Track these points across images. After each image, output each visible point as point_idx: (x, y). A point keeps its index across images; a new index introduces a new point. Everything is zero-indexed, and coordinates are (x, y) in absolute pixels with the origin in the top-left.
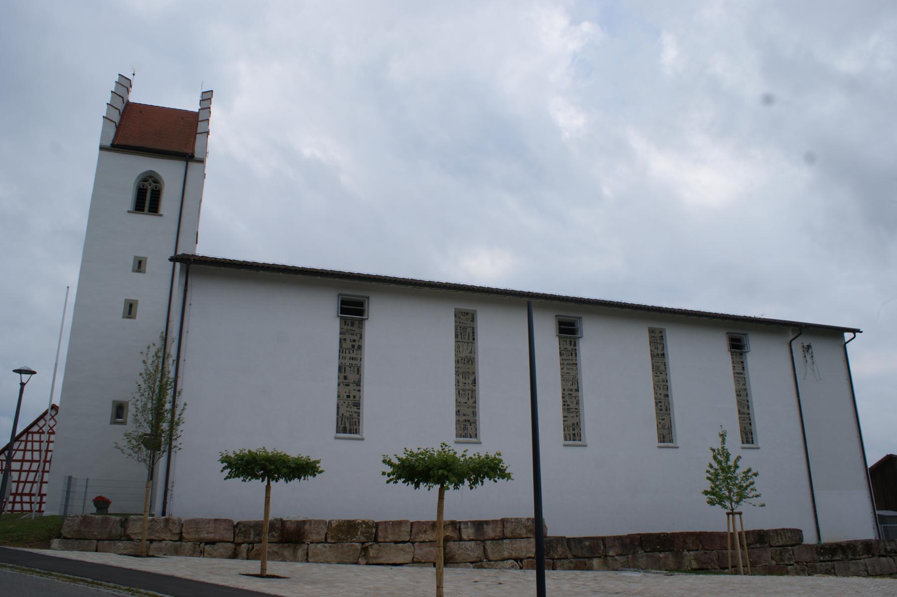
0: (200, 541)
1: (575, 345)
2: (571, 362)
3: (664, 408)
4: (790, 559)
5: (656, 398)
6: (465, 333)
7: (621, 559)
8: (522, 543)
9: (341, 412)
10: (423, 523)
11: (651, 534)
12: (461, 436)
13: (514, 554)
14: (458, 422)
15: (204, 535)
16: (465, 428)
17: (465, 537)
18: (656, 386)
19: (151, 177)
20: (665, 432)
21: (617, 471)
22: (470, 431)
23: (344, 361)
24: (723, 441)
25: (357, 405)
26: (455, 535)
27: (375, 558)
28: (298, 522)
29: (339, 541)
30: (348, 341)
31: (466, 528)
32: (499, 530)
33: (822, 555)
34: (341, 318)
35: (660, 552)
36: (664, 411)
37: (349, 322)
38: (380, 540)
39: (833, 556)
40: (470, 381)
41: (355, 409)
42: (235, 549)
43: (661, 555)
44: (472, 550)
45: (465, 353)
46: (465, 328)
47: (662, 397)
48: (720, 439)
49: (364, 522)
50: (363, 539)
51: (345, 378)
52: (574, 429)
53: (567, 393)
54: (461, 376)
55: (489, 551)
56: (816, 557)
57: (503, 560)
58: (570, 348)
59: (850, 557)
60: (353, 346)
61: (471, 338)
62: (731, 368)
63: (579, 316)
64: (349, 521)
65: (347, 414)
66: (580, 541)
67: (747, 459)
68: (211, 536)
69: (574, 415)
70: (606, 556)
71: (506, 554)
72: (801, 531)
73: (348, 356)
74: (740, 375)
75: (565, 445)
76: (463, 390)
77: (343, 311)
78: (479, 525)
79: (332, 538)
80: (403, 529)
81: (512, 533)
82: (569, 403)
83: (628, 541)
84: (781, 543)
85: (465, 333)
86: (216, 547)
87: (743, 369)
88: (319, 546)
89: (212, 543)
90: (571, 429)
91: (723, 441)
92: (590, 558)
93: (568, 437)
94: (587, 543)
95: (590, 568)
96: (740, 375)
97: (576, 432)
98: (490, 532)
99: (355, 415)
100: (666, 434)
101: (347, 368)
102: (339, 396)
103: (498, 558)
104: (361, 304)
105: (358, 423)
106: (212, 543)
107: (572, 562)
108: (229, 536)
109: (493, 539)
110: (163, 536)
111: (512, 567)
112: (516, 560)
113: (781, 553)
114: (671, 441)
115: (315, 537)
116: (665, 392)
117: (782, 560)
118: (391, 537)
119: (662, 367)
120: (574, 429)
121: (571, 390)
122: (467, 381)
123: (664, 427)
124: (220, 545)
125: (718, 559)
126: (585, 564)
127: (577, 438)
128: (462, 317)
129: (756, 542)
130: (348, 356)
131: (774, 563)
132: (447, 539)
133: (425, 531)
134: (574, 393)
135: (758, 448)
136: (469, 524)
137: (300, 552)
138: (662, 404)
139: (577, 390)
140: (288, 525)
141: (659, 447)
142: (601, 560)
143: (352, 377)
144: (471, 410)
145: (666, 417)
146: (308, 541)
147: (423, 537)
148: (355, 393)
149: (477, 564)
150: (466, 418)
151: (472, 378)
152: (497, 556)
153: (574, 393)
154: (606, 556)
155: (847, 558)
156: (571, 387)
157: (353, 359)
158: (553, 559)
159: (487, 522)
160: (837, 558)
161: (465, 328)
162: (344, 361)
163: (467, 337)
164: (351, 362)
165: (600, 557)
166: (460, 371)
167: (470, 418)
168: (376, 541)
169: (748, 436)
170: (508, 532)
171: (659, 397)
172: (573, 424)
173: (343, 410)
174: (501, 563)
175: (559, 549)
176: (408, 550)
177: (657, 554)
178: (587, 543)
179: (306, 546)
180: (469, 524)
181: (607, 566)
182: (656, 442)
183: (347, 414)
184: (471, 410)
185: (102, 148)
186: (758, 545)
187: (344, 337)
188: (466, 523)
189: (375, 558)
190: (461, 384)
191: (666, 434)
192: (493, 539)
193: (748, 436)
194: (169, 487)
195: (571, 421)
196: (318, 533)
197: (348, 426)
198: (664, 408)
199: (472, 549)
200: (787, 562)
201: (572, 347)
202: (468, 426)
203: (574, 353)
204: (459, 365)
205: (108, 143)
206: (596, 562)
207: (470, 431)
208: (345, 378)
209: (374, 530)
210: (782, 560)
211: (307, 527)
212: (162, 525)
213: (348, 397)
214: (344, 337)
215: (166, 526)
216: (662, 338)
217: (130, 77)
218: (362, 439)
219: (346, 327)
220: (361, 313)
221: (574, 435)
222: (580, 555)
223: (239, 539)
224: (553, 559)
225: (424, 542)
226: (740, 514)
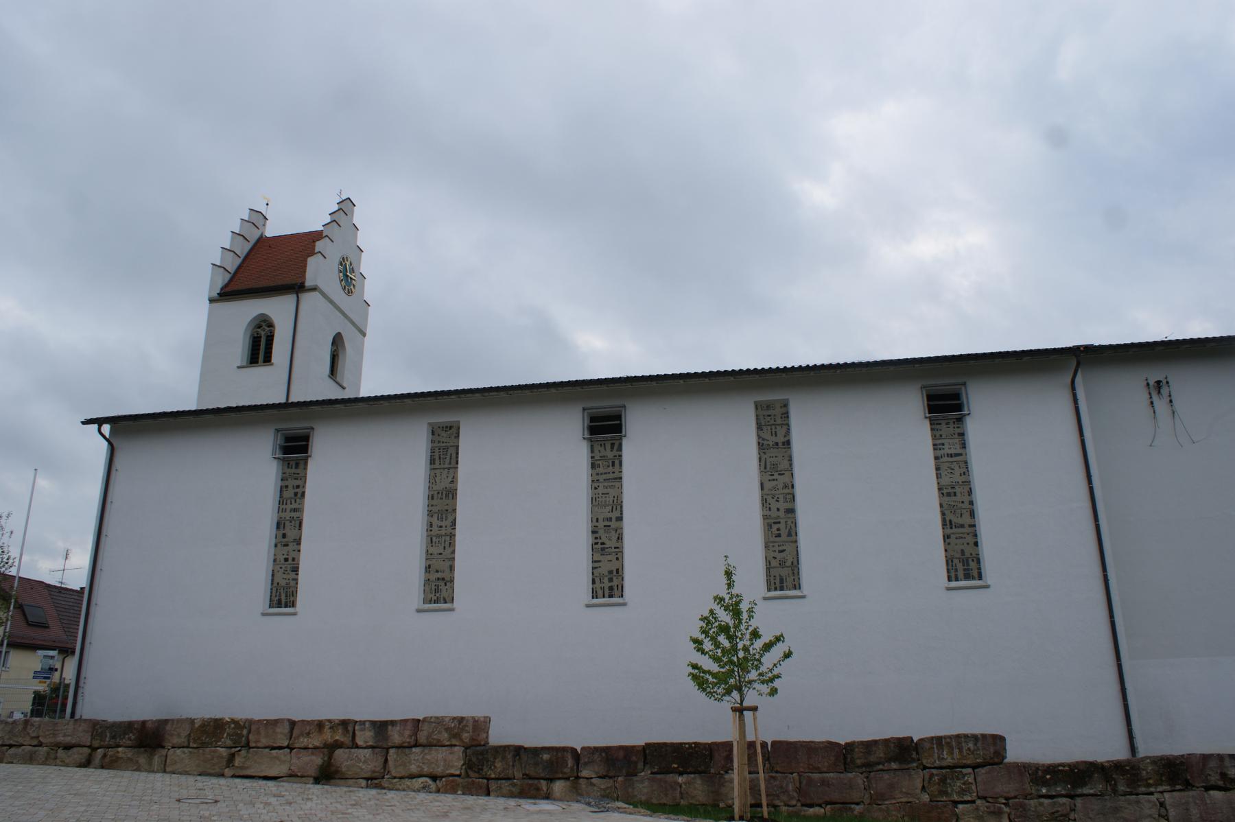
0: (58, 745)
1: (620, 449)
2: (612, 476)
3: (784, 532)
4: (962, 792)
5: (765, 517)
6: (444, 455)
7: (603, 784)
8: (439, 754)
9: (276, 580)
10: (308, 722)
11: (665, 744)
12: (430, 602)
13: (426, 770)
14: (427, 581)
15: (60, 739)
16: (437, 590)
17: (360, 742)
18: (945, 492)
19: (265, 321)
20: (784, 572)
21: (559, 647)
22: (444, 594)
23: (283, 515)
24: (730, 585)
25: (296, 570)
26: (346, 740)
27: (242, 768)
28: (159, 721)
29: (203, 745)
30: (290, 488)
31: (362, 730)
32: (407, 733)
33: (1045, 783)
34: (930, 419)
35: (681, 774)
36: (784, 537)
37: (293, 463)
38: (252, 744)
39: (1074, 787)
40: (448, 523)
41: (293, 575)
42: (90, 755)
43: (680, 780)
44: (365, 762)
45: (443, 484)
46: (446, 449)
47: (782, 513)
48: (724, 580)
49: (233, 721)
50: (229, 743)
51: (284, 536)
52: (611, 580)
53: (601, 524)
54: (435, 516)
55: (391, 763)
56: (1029, 788)
57: (412, 777)
58: (610, 454)
59: (1122, 788)
60: (296, 494)
61: (453, 461)
62: (931, 448)
63: (960, 381)
64: (216, 720)
65: (283, 583)
66: (536, 752)
67: (770, 616)
68: (68, 739)
69: (613, 557)
70: (578, 777)
71: (414, 769)
72: (1002, 739)
73: (289, 507)
74: (291, 496)
75: (949, 589)
76: (438, 536)
77: (931, 409)
78: (381, 727)
79: (195, 741)
80: (278, 730)
81: (427, 738)
82: (604, 539)
83: (621, 754)
84: (949, 761)
85: (444, 455)
86: (71, 752)
87: (964, 446)
88: (178, 751)
89: (68, 747)
90: (606, 580)
91: (730, 585)
92: (551, 780)
93: (600, 593)
94: (546, 757)
95: (548, 797)
96: (291, 496)
97: (614, 583)
98: (396, 736)
99: (292, 583)
100: (608, 583)
101: (287, 523)
102: (275, 560)
103: (403, 773)
104: (957, 396)
105: (294, 593)
106: (68, 747)
107: (514, 785)
108: (86, 739)
109: (397, 747)
110: (20, 740)
111: (425, 788)
112: (434, 778)
113: (943, 780)
114: (797, 586)
115: (176, 740)
116: (789, 506)
117: (943, 793)
118: (264, 741)
119: (785, 464)
120: (611, 580)
121: (610, 519)
122: (443, 524)
123: (782, 564)
124: (75, 750)
125: (799, 790)
126: (538, 789)
127: (616, 592)
128: (443, 434)
129: (889, 760)
130: (289, 507)
131: (926, 798)
132: (333, 747)
133: (308, 734)
134: (613, 524)
135: (987, 587)
136: (367, 725)
137: (156, 759)
138: (782, 526)
139: (620, 519)
140: (149, 725)
141: (949, 589)
142: (568, 783)
143: (291, 534)
144: (448, 563)
145: (787, 547)
146: (168, 745)
147: (304, 741)
148: (293, 554)
149: (374, 781)
150: (439, 575)
151: (450, 519)
152: (402, 771)
153: (613, 524)
154: (578, 777)
155: (1115, 791)
156: (610, 515)
157: (294, 510)
158: (488, 779)
159: (393, 723)
160: (1086, 791)
161: (446, 449)
162: (283, 515)
163: (448, 460)
164: (293, 514)
165: (567, 779)
166: (435, 509)
167: (446, 575)
168: (247, 746)
169: (783, 574)
170: (422, 738)
171: (774, 513)
172: (611, 572)
173: (278, 579)
174: (407, 782)
175: (498, 765)
176: (283, 758)
177: (671, 777)
178: (546, 757)
179: (164, 752)
180: (367, 725)
181: (576, 792)
182: (586, 596)
183: (283, 583)
184: (448, 563)
185: (211, 301)
186: (894, 766)
187: (286, 483)
188: (363, 723)
189: (242, 768)
190: (435, 528)
191: (608, 583)
192: (397, 747)
193: (783, 574)
194: (81, 684)
195: (605, 568)
196: (179, 735)
197: (283, 597)
198: (784, 532)
199: (365, 760)
200: (956, 798)
201: (615, 452)
202: (443, 587)
203: (617, 461)
204: (434, 502)
205: (215, 294)
206: (559, 787)
207: (444, 594)
208: (284, 536)
209: (245, 732)
210: (943, 793)
211: (168, 727)
212: (20, 727)
213: (286, 560)
214: (286, 483)
215: (25, 728)
216: (786, 415)
217: (262, 209)
218: (987, 587)
219: (289, 471)
220: (959, 408)
221: (611, 588)
222: (532, 774)
223: (96, 744)
224: (488, 779)
225: (306, 748)
226: (754, 709)
